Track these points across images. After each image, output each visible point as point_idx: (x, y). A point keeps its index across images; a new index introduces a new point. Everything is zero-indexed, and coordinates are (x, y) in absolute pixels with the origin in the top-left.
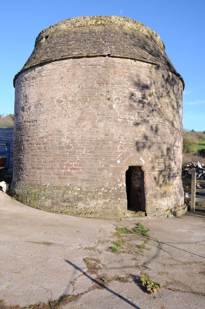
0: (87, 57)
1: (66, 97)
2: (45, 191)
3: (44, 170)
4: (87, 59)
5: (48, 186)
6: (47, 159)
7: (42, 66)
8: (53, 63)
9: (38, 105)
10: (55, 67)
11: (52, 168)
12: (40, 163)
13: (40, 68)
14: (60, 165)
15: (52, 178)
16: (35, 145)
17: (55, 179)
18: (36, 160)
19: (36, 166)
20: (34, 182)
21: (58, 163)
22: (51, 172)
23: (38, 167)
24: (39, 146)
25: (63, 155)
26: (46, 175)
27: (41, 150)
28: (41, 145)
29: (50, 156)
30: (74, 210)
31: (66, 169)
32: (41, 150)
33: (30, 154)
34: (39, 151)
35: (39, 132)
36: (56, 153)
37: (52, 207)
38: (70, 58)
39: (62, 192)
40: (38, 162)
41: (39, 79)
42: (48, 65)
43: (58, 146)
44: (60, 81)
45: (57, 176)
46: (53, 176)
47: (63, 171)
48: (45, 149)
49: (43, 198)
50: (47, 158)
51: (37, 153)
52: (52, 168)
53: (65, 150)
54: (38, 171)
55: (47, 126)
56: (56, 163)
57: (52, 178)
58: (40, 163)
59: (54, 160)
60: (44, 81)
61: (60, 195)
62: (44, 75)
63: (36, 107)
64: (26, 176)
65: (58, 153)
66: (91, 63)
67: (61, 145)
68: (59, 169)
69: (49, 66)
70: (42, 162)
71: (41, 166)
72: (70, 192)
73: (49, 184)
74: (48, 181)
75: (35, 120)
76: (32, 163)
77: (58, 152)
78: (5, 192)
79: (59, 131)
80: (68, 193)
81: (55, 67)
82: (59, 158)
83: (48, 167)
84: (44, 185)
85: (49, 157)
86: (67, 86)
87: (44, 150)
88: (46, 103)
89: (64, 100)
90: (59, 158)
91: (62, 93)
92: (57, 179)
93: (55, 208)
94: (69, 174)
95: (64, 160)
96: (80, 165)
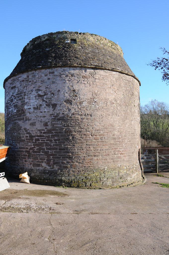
0: (127, 74)
1: (116, 101)
2: (105, 174)
3: (101, 157)
4: (126, 75)
5: (106, 169)
6: (104, 148)
7: (95, 70)
8: (105, 70)
9: (92, 101)
10: (107, 74)
11: (108, 155)
12: (97, 151)
13: (93, 71)
14: (114, 151)
15: (108, 162)
16: (90, 136)
17: (110, 163)
18: (92, 148)
19: (93, 154)
20: (91, 167)
21: (113, 150)
22: (107, 158)
23: (95, 154)
24: (95, 137)
25: (116, 144)
26: (103, 161)
27: (98, 140)
28: (97, 136)
29: (106, 145)
30: (126, 184)
31: (118, 154)
32: (97, 140)
33: (85, 144)
34: (95, 141)
35: (94, 125)
36: (111, 143)
37: (113, 185)
38: (117, 72)
39: (117, 171)
40: (94, 151)
41: (91, 80)
42: (101, 71)
43: (112, 137)
44: (111, 87)
45: (112, 161)
46: (109, 160)
47: (116, 156)
48: (101, 139)
49: (105, 180)
50: (104, 147)
51: (93, 143)
52: (108, 155)
53: (117, 140)
54: (96, 158)
55: (103, 121)
56: (111, 150)
57: (108, 162)
58: (97, 151)
59: (109, 148)
60: (97, 83)
61: (117, 174)
62: (97, 78)
63: (90, 103)
64: (77, 164)
65: (112, 143)
66: (128, 79)
67: (114, 137)
68: (113, 154)
69: (102, 72)
70: (99, 150)
71: (98, 154)
72: (122, 171)
73: (106, 167)
74: (105, 166)
75: (89, 114)
76: (88, 151)
77: (112, 142)
78: (29, 183)
79: (112, 125)
80: (121, 172)
81: (107, 74)
82: (113, 146)
83: (104, 154)
84: (103, 168)
85: (106, 146)
86: (116, 92)
87: (100, 140)
88: (101, 102)
89: (115, 102)
90: (113, 146)
91: (113, 96)
92: (112, 163)
93: (115, 185)
94: (119, 157)
95: (116, 147)
96: (125, 151)
